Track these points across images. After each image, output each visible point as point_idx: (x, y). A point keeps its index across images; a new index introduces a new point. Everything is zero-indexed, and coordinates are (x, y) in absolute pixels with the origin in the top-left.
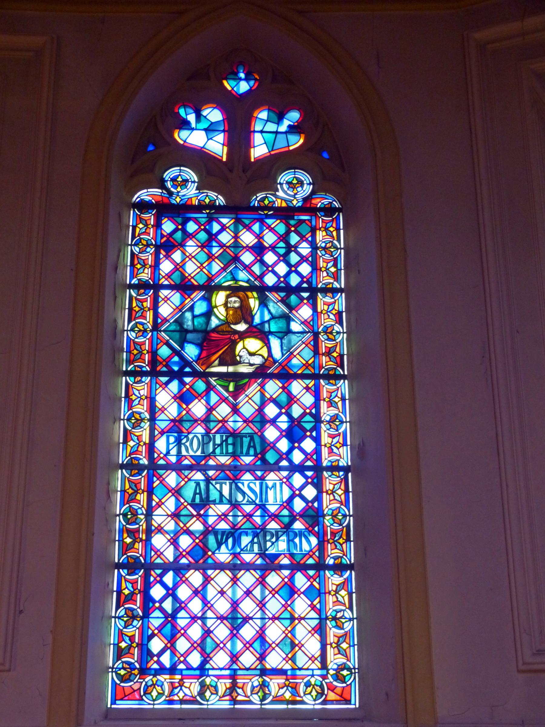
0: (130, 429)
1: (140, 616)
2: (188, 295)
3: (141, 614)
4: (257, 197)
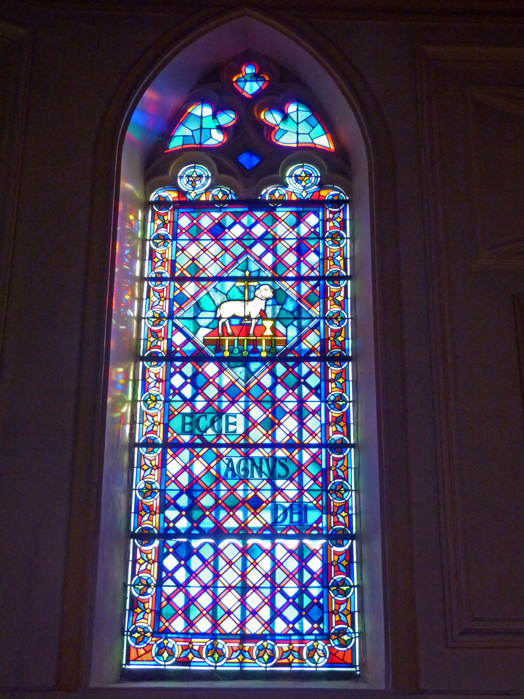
0: (137, 595)
2: (199, 366)
4: (268, 191)
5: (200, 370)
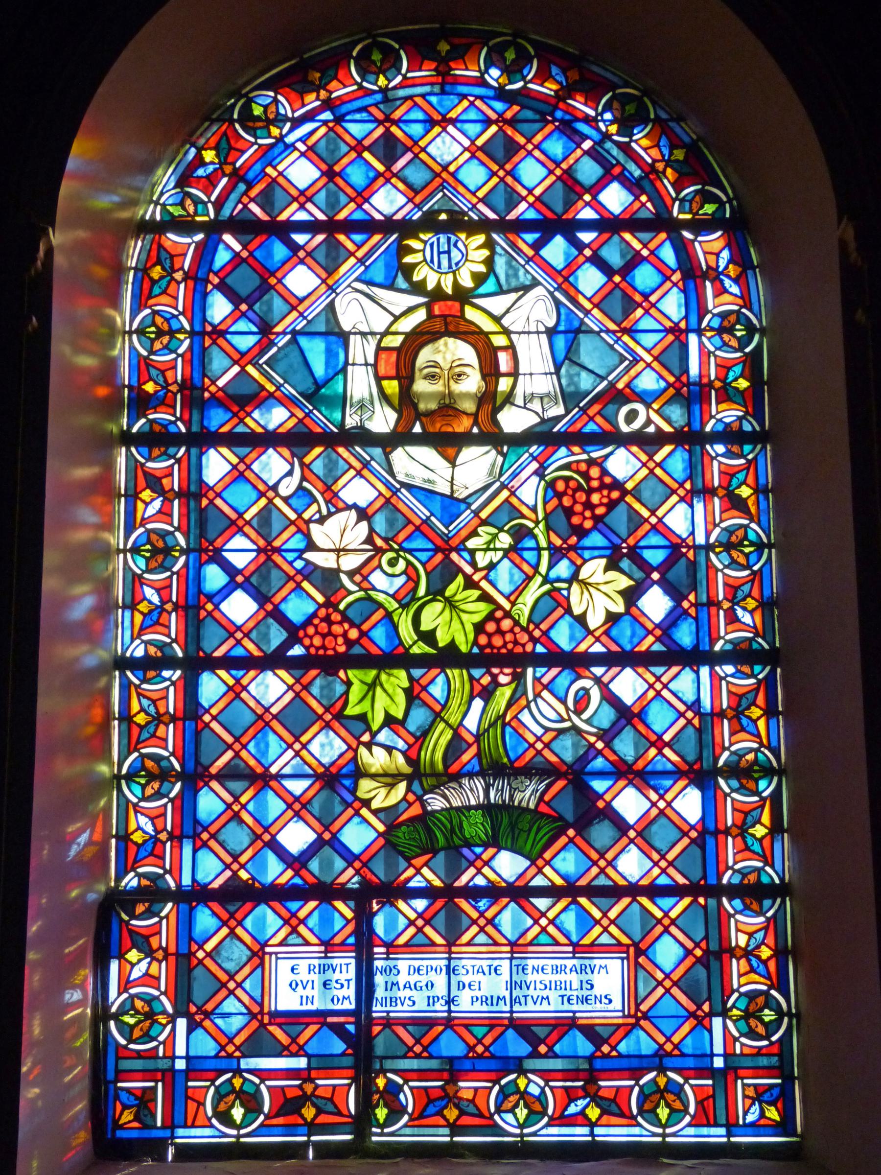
1: (182, 547)
3: (170, 1009)
5: (617, 279)
